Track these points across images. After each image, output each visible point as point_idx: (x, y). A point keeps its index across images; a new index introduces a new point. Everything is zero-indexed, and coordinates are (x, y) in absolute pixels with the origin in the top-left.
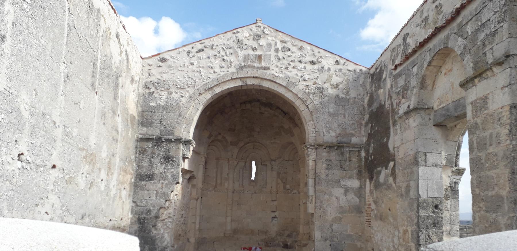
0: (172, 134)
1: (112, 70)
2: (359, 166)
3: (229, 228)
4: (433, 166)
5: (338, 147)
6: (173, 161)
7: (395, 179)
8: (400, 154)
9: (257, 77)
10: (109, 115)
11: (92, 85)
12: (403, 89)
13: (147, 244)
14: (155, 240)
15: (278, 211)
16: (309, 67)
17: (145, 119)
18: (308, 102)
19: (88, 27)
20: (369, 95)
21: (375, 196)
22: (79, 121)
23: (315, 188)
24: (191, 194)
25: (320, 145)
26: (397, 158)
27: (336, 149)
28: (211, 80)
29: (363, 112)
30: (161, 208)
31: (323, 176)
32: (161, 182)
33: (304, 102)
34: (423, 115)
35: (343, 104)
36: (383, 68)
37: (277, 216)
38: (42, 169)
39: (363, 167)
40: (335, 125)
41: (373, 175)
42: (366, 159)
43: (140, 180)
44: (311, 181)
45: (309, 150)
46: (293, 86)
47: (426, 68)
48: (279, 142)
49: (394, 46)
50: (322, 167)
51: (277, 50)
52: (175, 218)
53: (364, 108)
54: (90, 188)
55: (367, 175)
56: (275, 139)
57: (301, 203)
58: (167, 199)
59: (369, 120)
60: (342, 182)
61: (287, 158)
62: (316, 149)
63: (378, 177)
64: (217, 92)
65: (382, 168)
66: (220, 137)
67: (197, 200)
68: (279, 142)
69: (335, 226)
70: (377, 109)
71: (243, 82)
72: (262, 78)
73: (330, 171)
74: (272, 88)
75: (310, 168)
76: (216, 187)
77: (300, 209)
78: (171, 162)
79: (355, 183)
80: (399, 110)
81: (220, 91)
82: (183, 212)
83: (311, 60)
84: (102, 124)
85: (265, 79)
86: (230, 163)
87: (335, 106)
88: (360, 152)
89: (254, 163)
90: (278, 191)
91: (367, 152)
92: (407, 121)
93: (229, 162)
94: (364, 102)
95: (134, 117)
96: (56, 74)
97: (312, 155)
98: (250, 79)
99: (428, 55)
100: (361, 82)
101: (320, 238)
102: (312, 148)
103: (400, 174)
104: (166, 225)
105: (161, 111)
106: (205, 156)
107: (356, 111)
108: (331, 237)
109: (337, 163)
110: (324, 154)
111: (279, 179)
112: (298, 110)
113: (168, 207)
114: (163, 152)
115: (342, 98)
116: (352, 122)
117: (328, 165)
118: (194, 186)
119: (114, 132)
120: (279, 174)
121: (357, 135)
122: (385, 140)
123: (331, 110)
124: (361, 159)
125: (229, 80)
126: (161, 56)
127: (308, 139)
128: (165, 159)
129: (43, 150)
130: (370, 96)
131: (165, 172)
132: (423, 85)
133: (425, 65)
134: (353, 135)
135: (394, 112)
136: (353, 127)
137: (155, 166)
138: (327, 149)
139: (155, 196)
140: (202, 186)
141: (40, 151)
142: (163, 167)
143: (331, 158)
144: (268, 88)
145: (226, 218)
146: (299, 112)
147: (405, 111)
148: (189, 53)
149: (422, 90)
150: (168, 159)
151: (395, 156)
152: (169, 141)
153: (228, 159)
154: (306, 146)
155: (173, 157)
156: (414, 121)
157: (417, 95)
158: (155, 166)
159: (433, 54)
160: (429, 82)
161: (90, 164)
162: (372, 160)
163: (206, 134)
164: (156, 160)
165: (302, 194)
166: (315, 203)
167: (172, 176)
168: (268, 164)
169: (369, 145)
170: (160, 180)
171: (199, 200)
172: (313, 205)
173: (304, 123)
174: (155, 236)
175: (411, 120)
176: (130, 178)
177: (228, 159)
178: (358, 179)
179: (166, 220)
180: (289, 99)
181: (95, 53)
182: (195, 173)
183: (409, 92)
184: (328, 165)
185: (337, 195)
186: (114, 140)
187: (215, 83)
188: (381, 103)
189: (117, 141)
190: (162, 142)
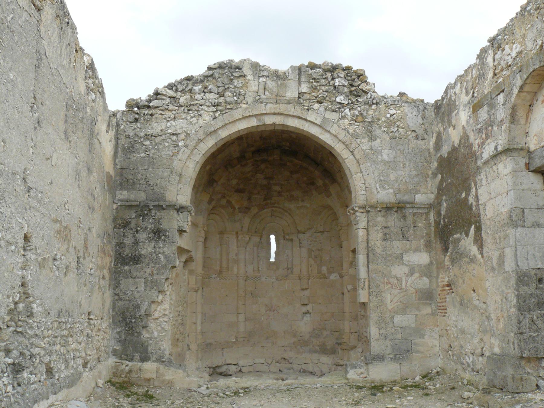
0: (163, 198)
1: (86, 112)
2: (428, 235)
3: (242, 329)
4: (533, 225)
6: (166, 236)
7: (481, 248)
8: (487, 213)
9: (279, 114)
10: (84, 174)
11: (65, 132)
12: (486, 123)
13: (137, 352)
14: (147, 346)
15: (310, 304)
17: (123, 178)
18: (353, 146)
19: (60, 55)
20: (435, 135)
22: (51, 183)
23: (368, 267)
24: (188, 283)
25: (374, 207)
26: (483, 219)
27: (396, 212)
29: (428, 159)
30: (153, 302)
31: (379, 251)
33: (347, 147)
34: (516, 158)
36: (453, 98)
37: (311, 311)
38: (13, 247)
39: (433, 235)
41: (448, 245)
42: (437, 223)
44: (361, 259)
45: (358, 214)
46: (331, 124)
47: (517, 95)
48: (308, 205)
50: (376, 236)
52: (171, 315)
53: (429, 153)
54: (65, 274)
55: (439, 246)
56: (303, 201)
57: (345, 291)
58: (161, 289)
59: (437, 169)
60: (405, 258)
61: (321, 229)
62: (368, 212)
64: (223, 136)
65: (461, 234)
66: (224, 202)
67: (196, 292)
68: (308, 205)
70: (449, 153)
71: (260, 120)
72: (285, 115)
73: (388, 243)
74: (301, 128)
75: (360, 239)
76: (221, 272)
77: (343, 299)
78: (163, 237)
79: (422, 258)
80: (483, 152)
81: (228, 134)
82: (180, 308)
84: (76, 186)
85: (237, 120)
86: (240, 238)
87: (391, 151)
88: (427, 214)
89: (272, 237)
90: (309, 276)
91: (439, 213)
92: (495, 168)
93: (238, 237)
94: (429, 144)
95: (112, 176)
96: (26, 119)
97: (362, 220)
98: (269, 116)
99: (519, 78)
101: (377, 336)
102: (362, 211)
103: (489, 240)
104: (160, 325)
105: (146, 167)
106: (205, 229)
109: (398, 230)
110: (380, 219)
112: (339, 158)
113: (162, 302)
114: (151, 223)
117: (385, 234)
118: (191, 272)
119: (90, 197)
120: (310, 251)
121: (422, 190)
122: (463, 195)
123: (386, 157)
124: (430, 224)
125: (239, 119)
127: (356, 198)
128: (155, 233)
129: (14, 221)
131: (155, 252)
132: (513, 118)
133: (516, 91)
134: (418, 192)
135: (475, 157)
138: (382, 212)
139: (143, 286)
140: (203, 272)
141: (10, 223)
142: (153, 244)
143: (389, 224)
144: (296, 128)
145: (238, 317)
146: (341, 161)
147: (491, 154)
149: (513, 125)
150: (158, 233)
151: (479, 216)
152: (160, 207)
153: (237, 233)
154: (353, 209)
155: (165, 231)
156: (505, 167)
157: (508, 131)
159: (525, 76)
160: (521, 113)
161: (65, 241)
162: (445, 225)
163: (206, 198)
164: (142, 236)
165: (346, 278)
166: (369, 288)
169: (440, 204)
170: (149, 264)
171: (200, 292)
172: (367, 291)
173: (349, 177)
174: (148, 341)
175: (501, 166)
176: (108, 261)
177: (237, 233)
178: (426, 251)
179: (161, 319)
180: (325, 143)
181: (68, 90)
182: (193, 254)
183: (495, 128)
184: (385, 234)
186: (90, 208)
188: (453, 146)
189: (93, 209)
190: (150, 210)
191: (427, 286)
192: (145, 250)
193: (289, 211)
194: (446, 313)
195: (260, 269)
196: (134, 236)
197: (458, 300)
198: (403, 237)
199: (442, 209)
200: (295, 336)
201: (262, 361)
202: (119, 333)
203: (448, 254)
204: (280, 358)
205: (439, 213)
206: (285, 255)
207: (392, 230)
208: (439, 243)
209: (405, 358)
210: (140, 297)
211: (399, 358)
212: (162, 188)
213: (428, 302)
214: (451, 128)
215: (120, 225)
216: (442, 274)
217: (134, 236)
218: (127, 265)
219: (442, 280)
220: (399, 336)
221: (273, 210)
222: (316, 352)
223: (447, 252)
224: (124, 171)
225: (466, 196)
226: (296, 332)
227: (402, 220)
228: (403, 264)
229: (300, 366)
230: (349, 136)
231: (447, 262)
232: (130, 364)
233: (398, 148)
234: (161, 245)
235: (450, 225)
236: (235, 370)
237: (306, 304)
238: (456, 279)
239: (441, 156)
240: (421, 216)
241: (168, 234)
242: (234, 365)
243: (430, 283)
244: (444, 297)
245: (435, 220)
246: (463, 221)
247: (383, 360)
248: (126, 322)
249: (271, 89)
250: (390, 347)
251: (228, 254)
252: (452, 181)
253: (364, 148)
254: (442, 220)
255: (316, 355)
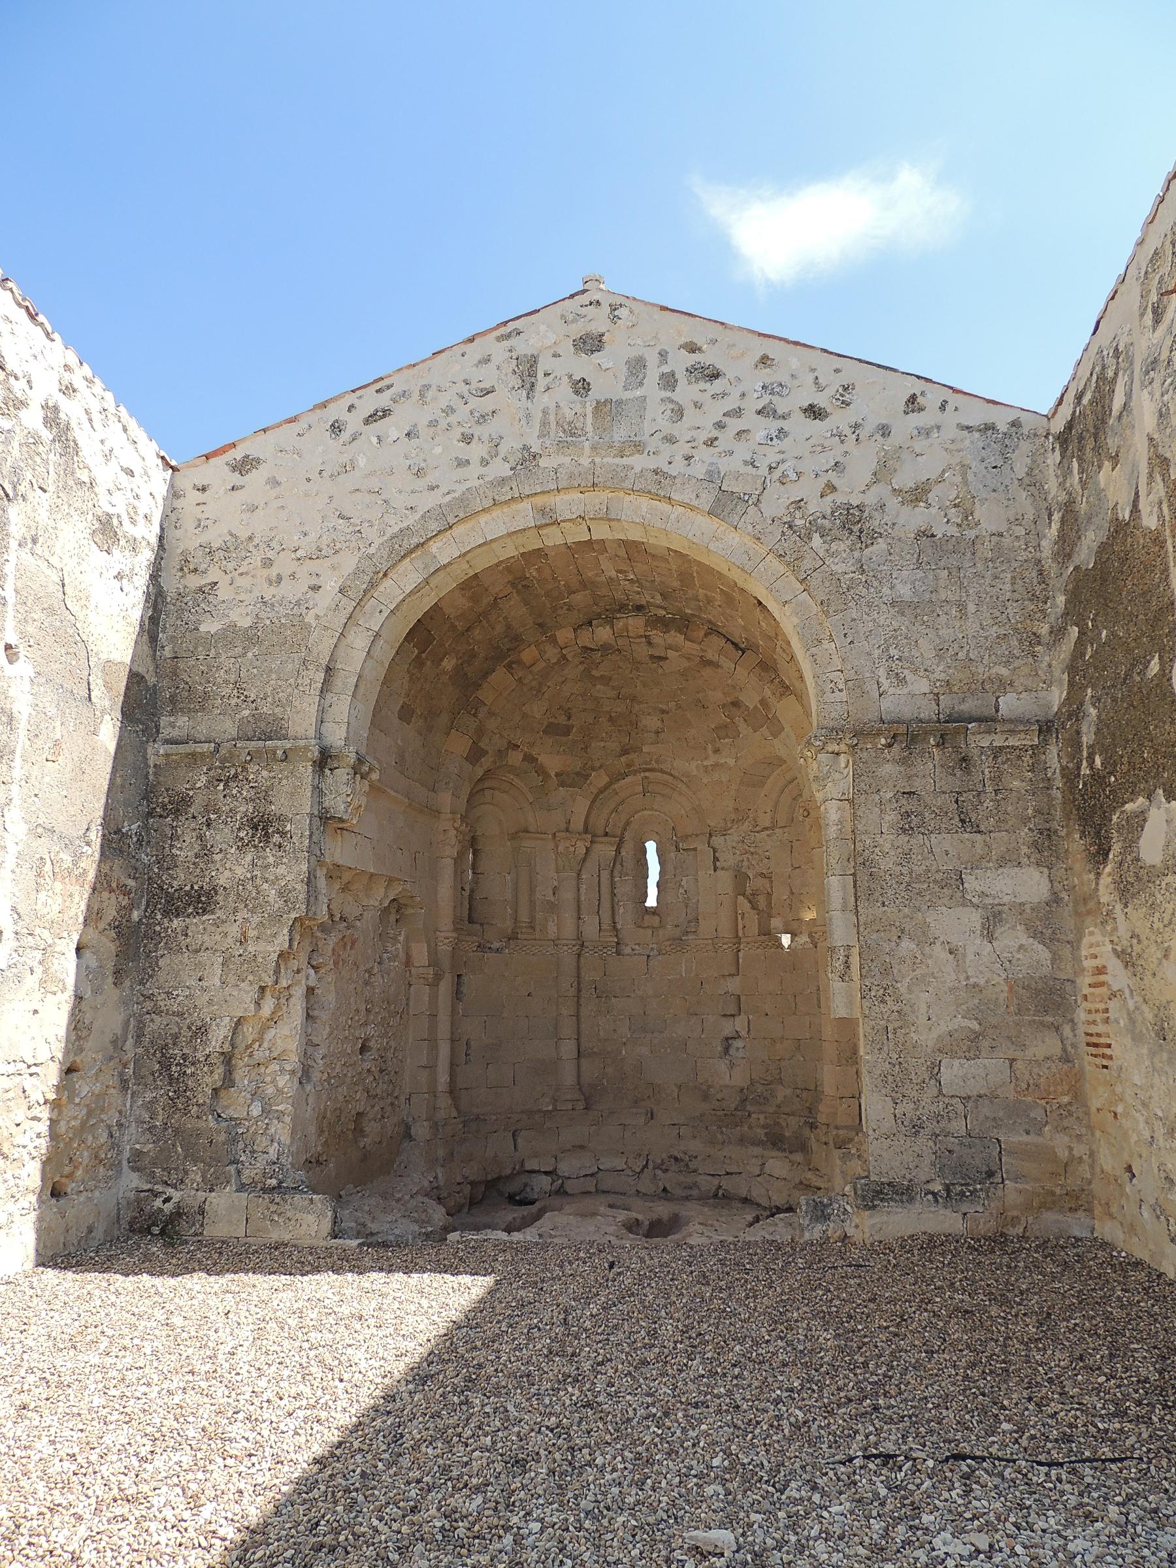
5: (944, 732)
6: (283, 834)
13: (195, 1162)
16: (800, 426)
20: (1056, 517)
21: (1123, 931)
28: (417, 516)
29: (1038, 589)
31: (887, 864)
32: (239, 916)
35: (953, 561)
39: (1058, 814)
40: (926, 649)
41: (1109, 838)
42: (1071, 776)
43: (166, 913)
46: (740, 509)
49: (1153, 244)
51: (669, 381)
53: (1041, 573)
55: (1076, 844)
56: (717, 751)
60: (972, 883)
63: (1131, 844)
66: (515, 758)
69: (953, 1072)
78: (276, 838)
79: (1029, 884)
83: (806, 405)
100: (1021, 471)
101: (889, 1124)
107: (1008, 587)
108: (938, 1117)
109: (947, 801)
111: (741, 898)
115: (947, 539)
116: (994, 631)
123: (905, 591)
126: (237, 454)
128: (255, 828)
130: (1063, 521)
134: (1004, 685)
136: (1002, 650)
137: (217, 857)
143: (917, 785)
148: (336, 428)
155: (280, 818)
158: (217, 857)
162: (1098, 778)
164: (221, 836)
167: (280, 894)
168: (702, 847)
170: (235, 910)
185: (956, 941)
187: (434, 526)
191: (1046, 971)
192: (227, 874)
193: (684, 779)
194: (1111, 1058)
195: (619, 927)
196: (200, 837)
197: (1149, 1016)
198: (963, 821)
199: (1084, 729)
200: (706, 1097)
201: (619, 1163)
202: (150, 1106)
203: (1108, 869)
204: (664, 1156)
205: (1075, 742)
206: (681, 891)
207: (928, 800)
208: (1077, 836)
209: (982, 1195)
210: (210, 1002)
211: (962, 1194)
212: (278, 703)
213: (1049, 1019)
214: (1107, 465)
215: (164, 807)
216: (1092, 933)
217: (200, 837)
218: (177, 916)
219: (1092, 951)
220: (958, 1126)
221: (646, 777)
222: (758, 1143)
223: (1105, 861)
224: (181, 665)
225: (1162, 669)
226: (709, 1087)
227: (958, 773)
228: (966, 902)
229: (716, 1181)
230: (795, 538)
231: (1106, 893)
232: (176, 1196)
233: (942, 564)
234: (271, 860)
235: (1110, 773)
236: (548, 1188)
237: (733, 1016)
238: (1137, 948)
239: (1077, 568)
240: (1019, 757)
241: (288, 828)
242: (546, 1173)
243: (1053, 961)
244: (1101, 1006)
245: (1063, 769)
246: (1156, 751)
247: (911, 1200)
248: (170, 1075)
249: (570, 423)
250: (929, 1158)
251: (532, 890)
252: (1113, 634)
253: (839, 568)
254: (1085, 763)
255: (757, 1150)
